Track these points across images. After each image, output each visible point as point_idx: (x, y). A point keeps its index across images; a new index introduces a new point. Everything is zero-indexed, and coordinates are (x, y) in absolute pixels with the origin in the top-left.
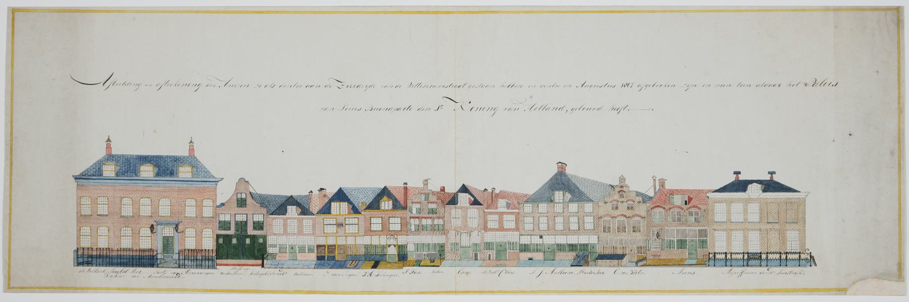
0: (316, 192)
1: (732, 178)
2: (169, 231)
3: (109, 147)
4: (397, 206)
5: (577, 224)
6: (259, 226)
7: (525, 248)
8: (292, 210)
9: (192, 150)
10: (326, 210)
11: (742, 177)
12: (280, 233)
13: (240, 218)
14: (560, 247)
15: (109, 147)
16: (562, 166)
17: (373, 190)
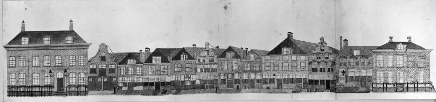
0: (144, 51)
1: (386, 41)
2: (60, 75)
3: (23, 27)
4: (190, 58)
5: (299, 67)
6: (112, 71)
7: (265, 81)
8: (157, 59)
9: (71, 26)
10: (149, 61)
11: (394, 40)
12: (127, 74)
13: (101, 67)
14: (286, 81)
15: (23, 27)
16: (290, 34)
17: (268, 51)
